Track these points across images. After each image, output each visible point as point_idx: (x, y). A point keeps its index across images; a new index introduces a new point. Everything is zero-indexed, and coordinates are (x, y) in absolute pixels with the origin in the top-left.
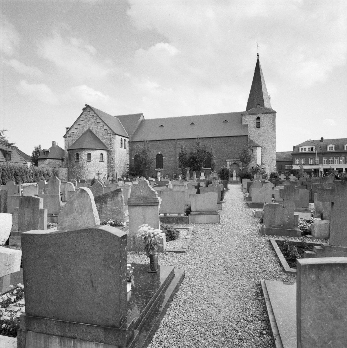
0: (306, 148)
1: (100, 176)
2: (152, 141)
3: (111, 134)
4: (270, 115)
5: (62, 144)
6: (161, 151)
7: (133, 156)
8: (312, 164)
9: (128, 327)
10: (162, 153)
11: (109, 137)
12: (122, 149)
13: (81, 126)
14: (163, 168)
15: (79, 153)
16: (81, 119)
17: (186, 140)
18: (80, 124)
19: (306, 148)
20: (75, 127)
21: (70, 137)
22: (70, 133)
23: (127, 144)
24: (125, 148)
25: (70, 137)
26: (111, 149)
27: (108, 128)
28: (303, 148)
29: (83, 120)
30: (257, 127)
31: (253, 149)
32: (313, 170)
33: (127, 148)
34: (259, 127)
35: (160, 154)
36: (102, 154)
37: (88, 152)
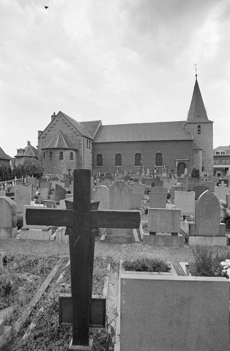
0: (219, 152)
1: (70, 172)
2: (112, 142)
3: (80, 136)
4: (208, 124)
5: (35, 144)
6: (120, 151)
7: (96, 155)
8: (224, 164)
9: (55, 189)
10: (120, 153)
11: (77, 138)
12: (88, 149)
13: (53, 129)
14: (121, 165)
15: (53, 152)
16: (53, 123)
17: (182, 142)
18: (52, 127)
19: (219, 152)
20: (48, 129)
21: (43, 138)
22: (43, 135)
23: (91, 145)
24: (90, 149)
25: (43, 138)
26: (79, 148)
27: (76, 131)
28: (222, 152)
29: (55, 124)
30: (198, 134)
31: (196, 151)
32: (224, 169)
33: (91, 148)
34: (200, 133)
35: (135, 156)
36: (72, 153)
37: (61, 151)
